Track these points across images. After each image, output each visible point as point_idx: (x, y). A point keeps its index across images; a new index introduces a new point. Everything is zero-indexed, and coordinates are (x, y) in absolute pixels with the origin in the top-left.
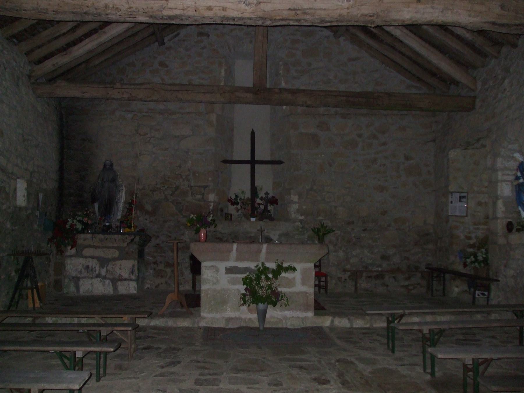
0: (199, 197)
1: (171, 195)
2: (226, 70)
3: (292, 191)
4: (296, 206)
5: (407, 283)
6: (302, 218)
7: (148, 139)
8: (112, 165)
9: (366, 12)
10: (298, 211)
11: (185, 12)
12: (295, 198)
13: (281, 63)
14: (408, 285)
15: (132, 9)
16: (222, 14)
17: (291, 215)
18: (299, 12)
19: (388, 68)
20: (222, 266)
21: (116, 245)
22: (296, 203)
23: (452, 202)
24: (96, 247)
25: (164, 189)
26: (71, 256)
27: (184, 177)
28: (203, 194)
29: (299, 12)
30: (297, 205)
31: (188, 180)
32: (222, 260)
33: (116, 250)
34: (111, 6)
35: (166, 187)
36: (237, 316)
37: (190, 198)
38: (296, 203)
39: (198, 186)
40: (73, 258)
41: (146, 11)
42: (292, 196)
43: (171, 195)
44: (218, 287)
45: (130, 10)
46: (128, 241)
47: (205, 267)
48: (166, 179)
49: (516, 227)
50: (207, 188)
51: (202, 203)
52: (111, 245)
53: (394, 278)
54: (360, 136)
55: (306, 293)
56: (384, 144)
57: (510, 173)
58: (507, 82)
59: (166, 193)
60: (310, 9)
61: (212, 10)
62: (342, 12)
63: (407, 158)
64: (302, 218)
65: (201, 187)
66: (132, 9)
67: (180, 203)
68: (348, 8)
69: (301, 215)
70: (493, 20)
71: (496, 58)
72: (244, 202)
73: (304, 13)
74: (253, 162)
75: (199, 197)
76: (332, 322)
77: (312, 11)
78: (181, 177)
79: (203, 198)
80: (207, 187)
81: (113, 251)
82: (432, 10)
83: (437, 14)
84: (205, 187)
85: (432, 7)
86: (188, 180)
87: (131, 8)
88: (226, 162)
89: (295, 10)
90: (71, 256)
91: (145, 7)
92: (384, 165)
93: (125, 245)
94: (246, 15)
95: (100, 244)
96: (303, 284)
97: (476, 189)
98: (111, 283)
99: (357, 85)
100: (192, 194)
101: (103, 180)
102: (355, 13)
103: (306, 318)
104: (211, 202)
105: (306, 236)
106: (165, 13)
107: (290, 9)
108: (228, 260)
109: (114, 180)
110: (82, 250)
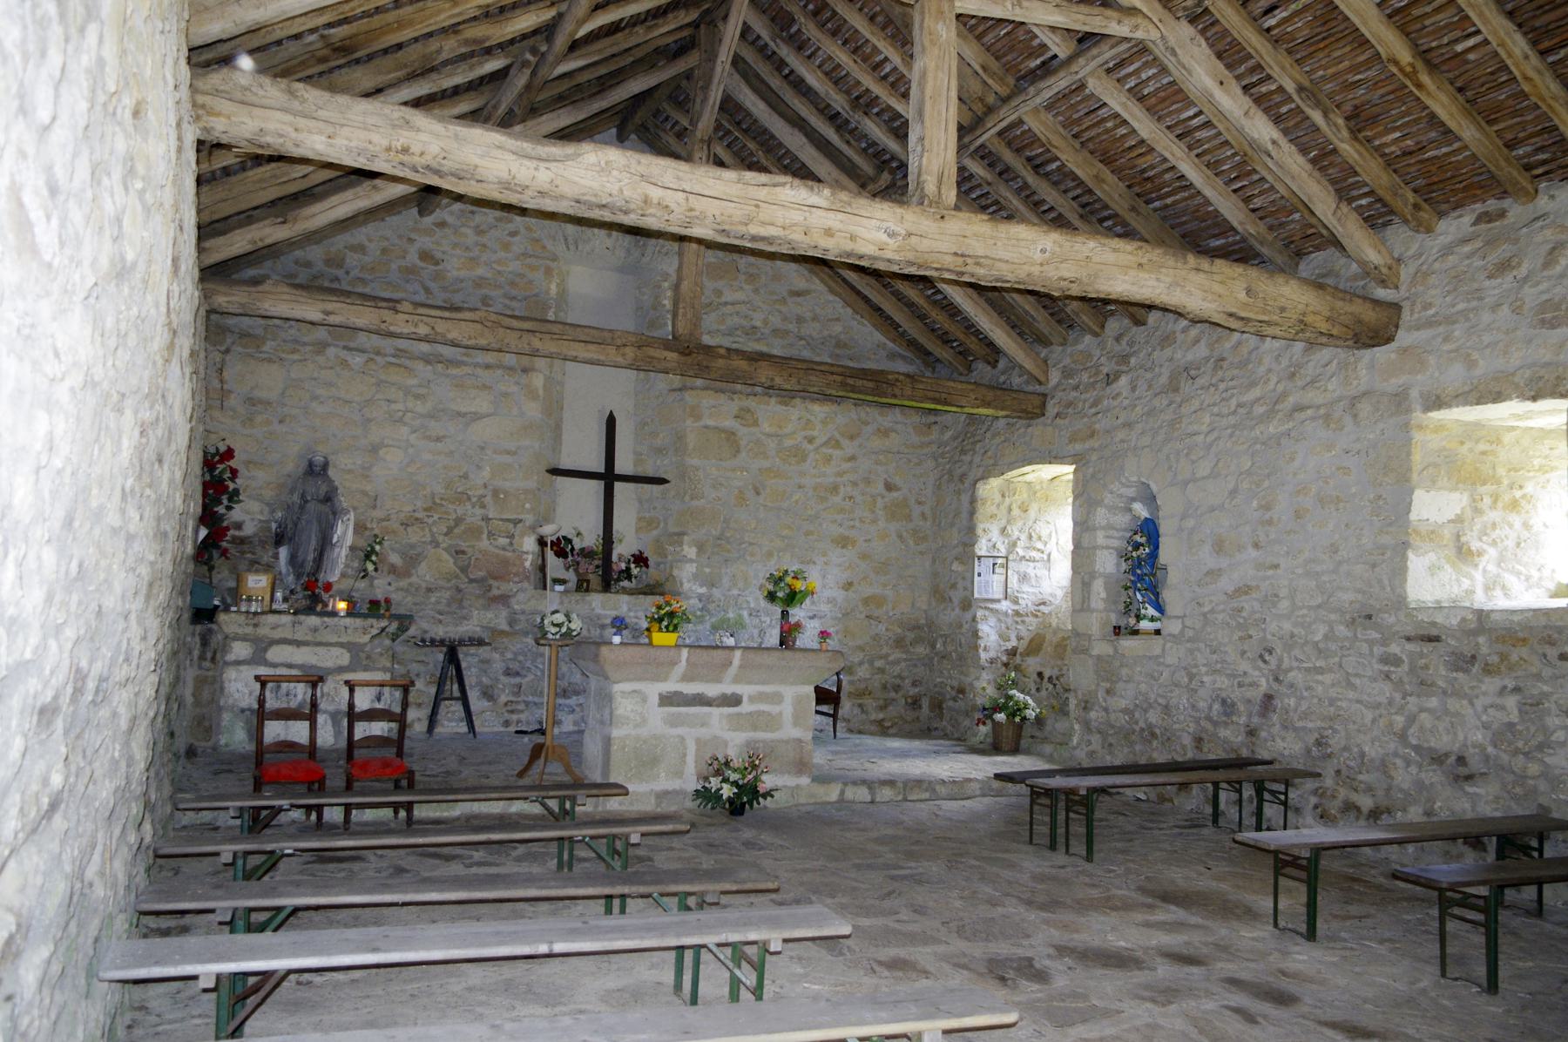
0: (503, 541)
1: (446, 535)
2: (558, 285)
3: (686, 538)
4: (690, 569)
5: (881, 716)
6: (703, 590)
7: (401, 414)
8: (325, 466)
9: (1067, 275)
10: (696, 577)
11: (787, 232)
12: (690, 551)
13: (666, 284)
14: (883, 720)
15: (693, 214)
16: (848, 246)
17: (682, 584)
18: (969, 261)
19: (858, 317)
20: (654, 690)
21: (344, 639)
22: (691, 561)
23: (979, 575)
24: (298, 644)
25: (430, 521)
26: (238, 663)
27: (474, 500)
28: (512, 537)
29: (969, 261)
30: (695, 565)
31: (483, 506)
32: (657, 678)
33: (344, 651)
34: (655, 201)
35: (436, 517)
36: (678, 788)
37: (484, 543)
38: (691, 561)
39: (502, 520)
40: (242, 668)
41: (718, 220)
42: (686, 548)
43: (446, 535)
44: (644, 732)
45: (688, 214)
46: (375, 631)
47: (622, 692)
48: (438, 501)
49: (1123, 631)
50: (520, 525)
51: (509, 554)
52: (334, 639)
53: (860, 706)
54: (811, 440)
55: (800, 741)
56: (852, 458)
57: (1116, 534)
58: (1124, 381)
59: (435, 530)
60: (986, 257)
61: (832, 236)
62: (1033, 269)
63: (889, 487)
64: (703, 590)
65: (508, 520)
66: (693, 214)
67: (463, 552)
68: (1041, 265)
69: (701, 586)
70: (1234, 310)
71: (1096, 335)
72: (586, 553)
73: (977, 264)
74: (609, 477)
75: (503, 541)
76: (842, 792)
77: (989, 262)
78: (469, 499)
79: (511, 544)
80: (521, 521)
81: (336, 651)
82: (1155, 284)
83: (1158, 291)
84: (516, 522)
85: (1158, 280)
86: (483, 506)
87: (691, 210)
88: (556, 472)
89: (962, 256)
90: (238, 663)
91: (717, 213)
92: (851, 498)
93: (367, 638)
94: (889, 255)
95: (309, 638)
96: (795, 724)
97: (1021, 553)
98: (329, 722)
99: (803, 342)
100: (490, 534)
101: (303, 496)
102: (1050, 275)
103: (798, 786)
104: (527, 553)
105: (708, 626)
106: (754, 230)
107: (956, 254)
108: (665, 680)
109: (328, 499)
110: (265, 650)
